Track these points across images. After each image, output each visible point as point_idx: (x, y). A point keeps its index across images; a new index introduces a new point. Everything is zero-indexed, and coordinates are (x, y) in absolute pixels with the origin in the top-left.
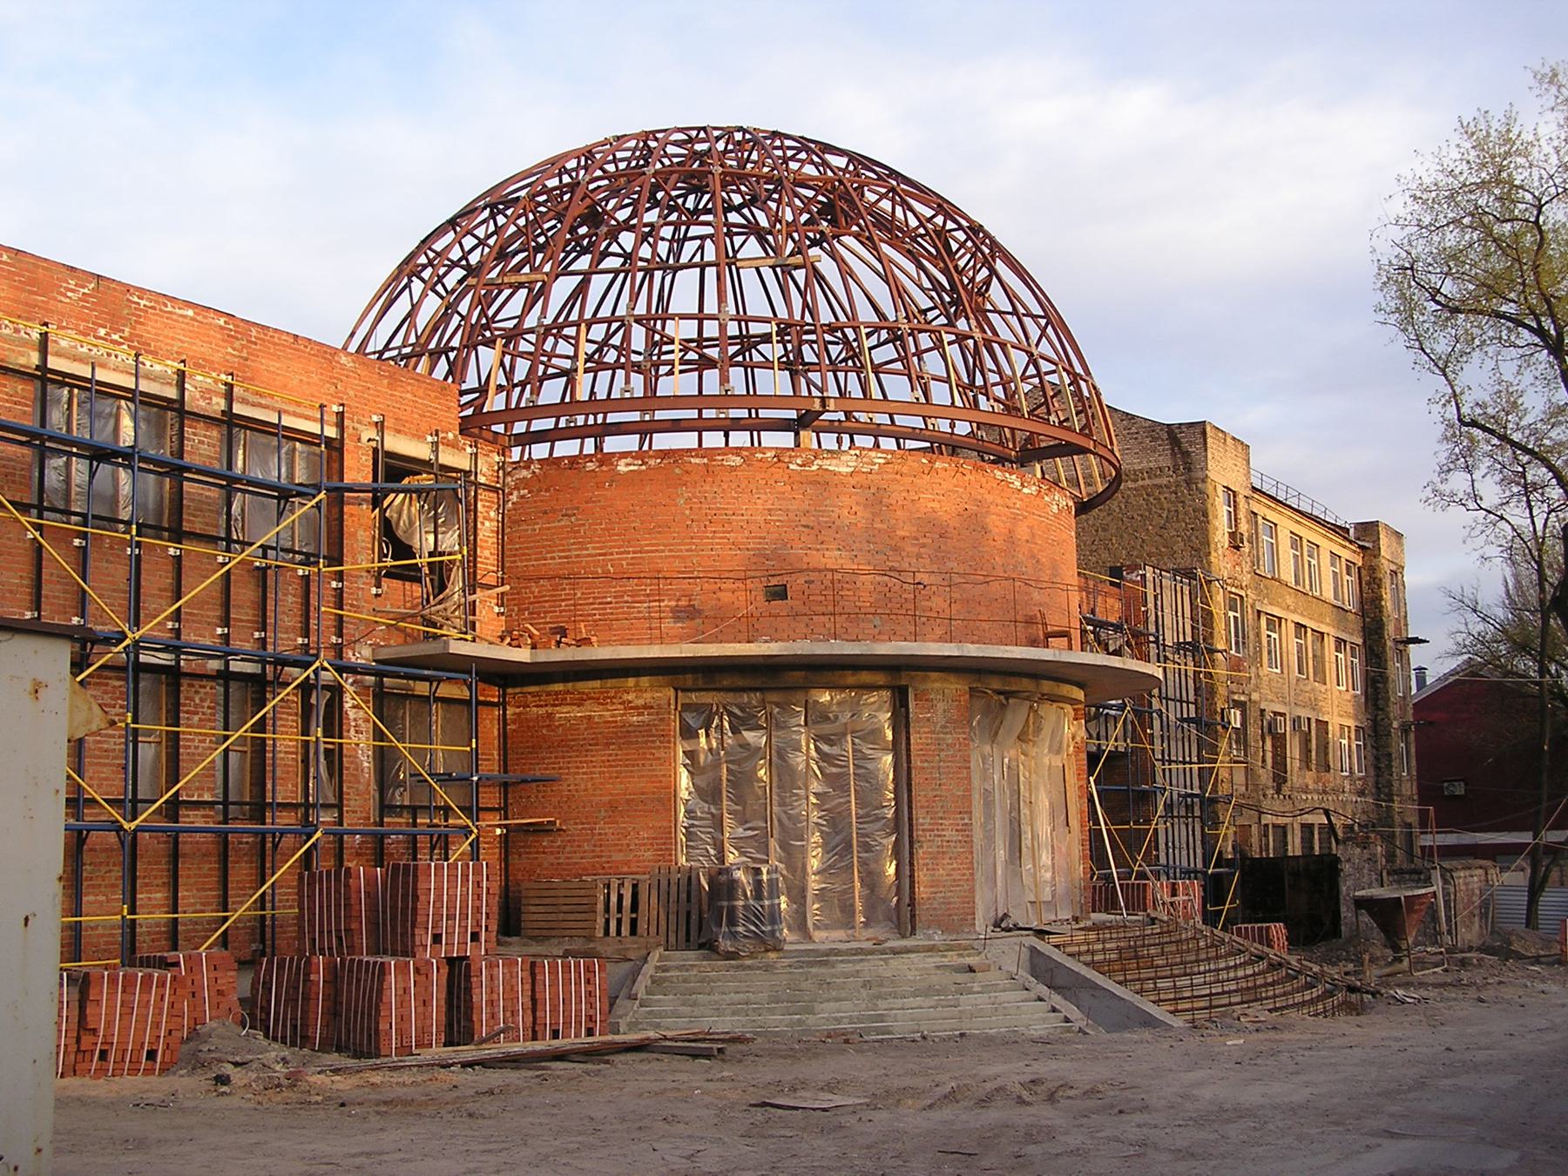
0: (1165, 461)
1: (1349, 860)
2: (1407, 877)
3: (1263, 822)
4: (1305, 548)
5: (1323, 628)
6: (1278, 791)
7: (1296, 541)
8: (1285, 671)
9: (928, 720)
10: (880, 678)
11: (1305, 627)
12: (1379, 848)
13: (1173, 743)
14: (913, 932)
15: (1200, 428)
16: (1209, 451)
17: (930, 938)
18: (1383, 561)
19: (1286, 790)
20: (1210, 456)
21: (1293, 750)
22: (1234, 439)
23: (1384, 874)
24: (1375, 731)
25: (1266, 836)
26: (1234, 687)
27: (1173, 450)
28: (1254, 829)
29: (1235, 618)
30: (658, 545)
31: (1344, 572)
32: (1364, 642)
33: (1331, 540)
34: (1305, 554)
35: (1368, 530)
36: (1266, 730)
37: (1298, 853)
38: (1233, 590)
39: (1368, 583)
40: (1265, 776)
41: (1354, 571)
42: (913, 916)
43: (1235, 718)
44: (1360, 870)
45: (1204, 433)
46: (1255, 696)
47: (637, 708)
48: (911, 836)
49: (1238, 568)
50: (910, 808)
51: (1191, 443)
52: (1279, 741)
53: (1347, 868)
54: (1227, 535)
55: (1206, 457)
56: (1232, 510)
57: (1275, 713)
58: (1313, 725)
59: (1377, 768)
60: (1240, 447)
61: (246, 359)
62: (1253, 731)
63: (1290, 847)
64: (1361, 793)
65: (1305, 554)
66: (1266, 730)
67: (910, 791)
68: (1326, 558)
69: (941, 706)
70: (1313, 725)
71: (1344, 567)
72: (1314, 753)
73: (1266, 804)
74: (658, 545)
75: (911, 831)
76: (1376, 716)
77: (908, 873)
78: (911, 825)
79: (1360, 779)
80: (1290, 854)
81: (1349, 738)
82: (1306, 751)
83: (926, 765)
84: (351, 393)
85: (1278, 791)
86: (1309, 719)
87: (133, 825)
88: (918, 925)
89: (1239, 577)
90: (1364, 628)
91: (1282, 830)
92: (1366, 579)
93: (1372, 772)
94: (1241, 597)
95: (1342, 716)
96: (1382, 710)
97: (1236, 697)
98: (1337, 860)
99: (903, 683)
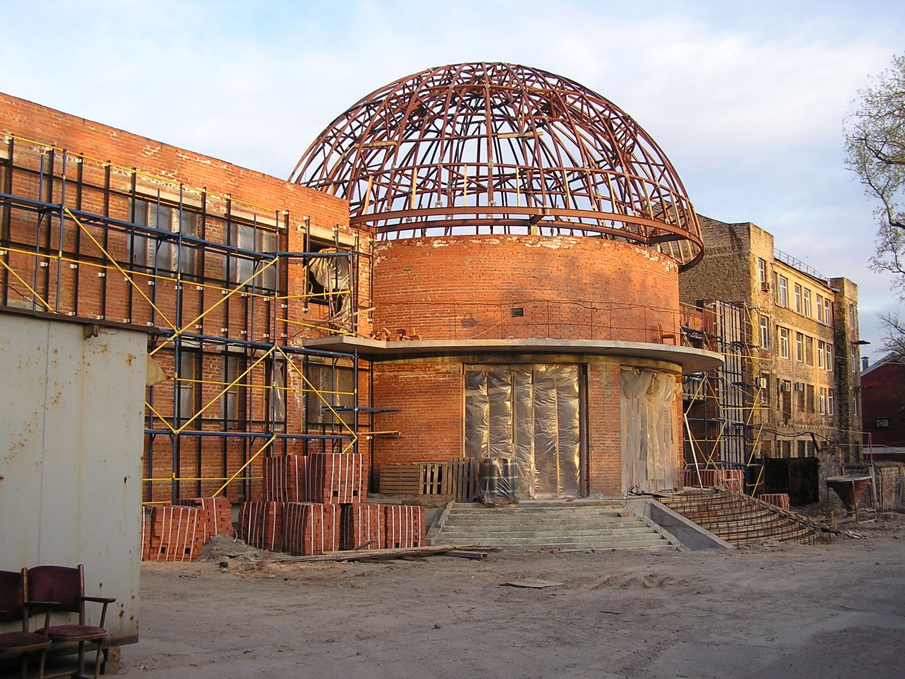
0: (728, 244)
1: (824, 461)
2: (856, 470)
3: (777, 439)
4: (803, 292)
5: (812, 335)
6: (786, 423)
7: (798, 287)
8: (791, 358)
10: (572, 359)
11: (802, 334)
12: (841, 455)
13: (729, 396)
14: (588, 495)
15: (746, 226)
16: (751, 238)
18: (846, 299)
19: (790, 422)
20: (752, 241)
21: (795, 401)
22: (765, 232)
23: (843, 469)
24: (840, 392)
25: (779, 447)
26: (763, 366)
27: (731, 238)
28: (773, 443)
29: (764, 329)
31: (824, 305)
32: (835, 343)
33: (818, 287)
34: (803, 295)
35: (838, 282)
36: (780, 390)
37: (796, 456)
38: (763, 314)
39: (837, 311)
40: (779, 414)
41: (830, 304)
42: (588, 486)
43: (763, 383)
44: (830, 466)
45: (749, 229)
46: (774, 371)
47: (442, 373)
48: (588, 444)
49: (766, 302)
50: (588, 429)
51: (741, 234)
52: (787, 396)
53: (823, 465)
54: (760, 284)
55: (750, 241)
56: (763, 270)
57: (785, 381)
58: (806, 387)
59: (840, 411)
60: (768, 237)
61: (238, 187)
62: (773, 390)
63: (792, 453)
64: (831, 425)
65: (803, 295)
66: (780, 390)
67: (587, 419)
68: (814, 297)
70: (806, 387)
71: (824, 302)
72: (806, 403)
73: (779, 429)
75: (588, 441)
76: (840, 383)
77: (586, 463)
78: (588, 438)
79: (830, 417)
80: (792, 457)
81: (825, 395)
82: (802, 401)
83: (596, 405)
85: (786, 423)
86: (803, 384)
87: (178, 431)
88: (591, 491)
89: (767, 307)
90: (834, 335)
91: (788, 444)
92: (836, 309)
93: (837, 413)
94: (768, 318)
95: (821, 383)
96: (843, 380)
97: (764, 372)
98: (817, 460)
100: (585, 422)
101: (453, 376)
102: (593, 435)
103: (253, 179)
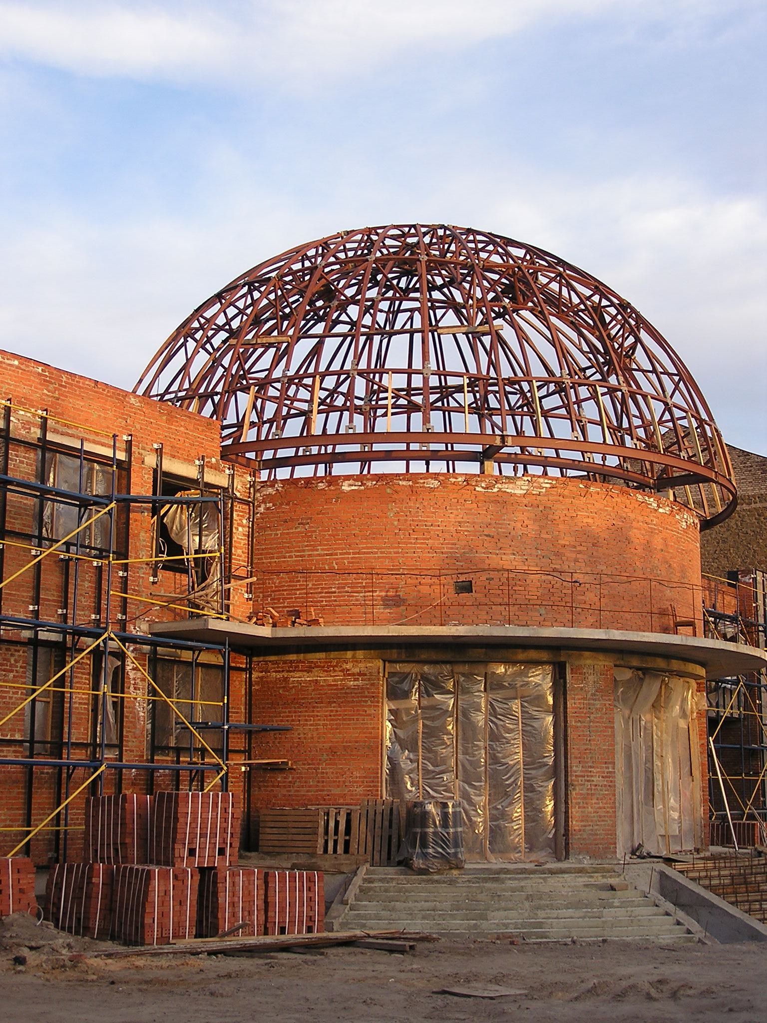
9: (582, 689)
10: (544, 656)
14: (567, 857)
17: (580, 862)
30: (371, 548)
42: (567, 844)
47: (353, 674)
48: (566, 780)
61: (58, 399)
67: (566, 745)
69: (591, 678)
74: (371, 548)
75: (566, 776)
83: (579, 724)
84: (138, 426)
88: (571, 851)
99: (562, 659)
100: (563, 749)
101: (369, 680)
102: (574, 768)
103: (80, 387)
